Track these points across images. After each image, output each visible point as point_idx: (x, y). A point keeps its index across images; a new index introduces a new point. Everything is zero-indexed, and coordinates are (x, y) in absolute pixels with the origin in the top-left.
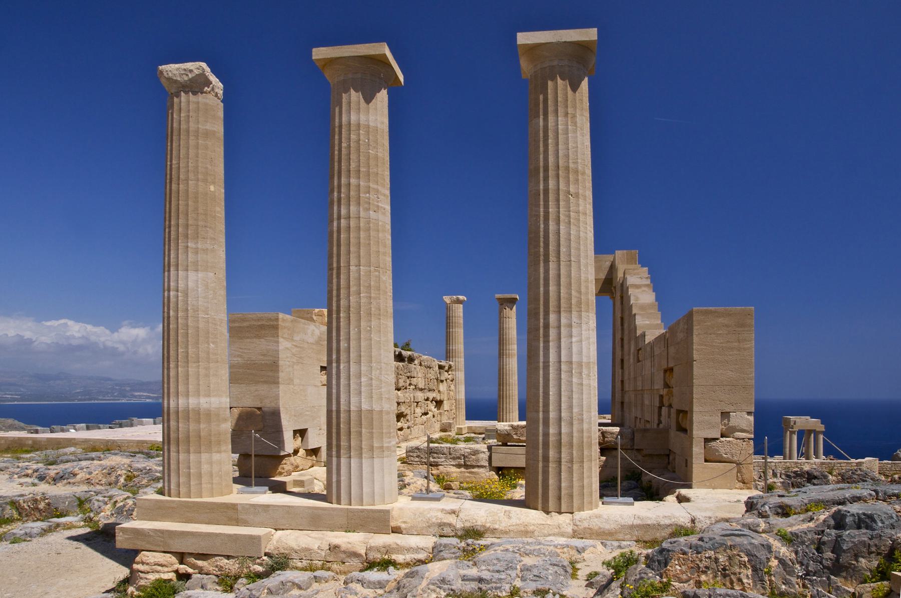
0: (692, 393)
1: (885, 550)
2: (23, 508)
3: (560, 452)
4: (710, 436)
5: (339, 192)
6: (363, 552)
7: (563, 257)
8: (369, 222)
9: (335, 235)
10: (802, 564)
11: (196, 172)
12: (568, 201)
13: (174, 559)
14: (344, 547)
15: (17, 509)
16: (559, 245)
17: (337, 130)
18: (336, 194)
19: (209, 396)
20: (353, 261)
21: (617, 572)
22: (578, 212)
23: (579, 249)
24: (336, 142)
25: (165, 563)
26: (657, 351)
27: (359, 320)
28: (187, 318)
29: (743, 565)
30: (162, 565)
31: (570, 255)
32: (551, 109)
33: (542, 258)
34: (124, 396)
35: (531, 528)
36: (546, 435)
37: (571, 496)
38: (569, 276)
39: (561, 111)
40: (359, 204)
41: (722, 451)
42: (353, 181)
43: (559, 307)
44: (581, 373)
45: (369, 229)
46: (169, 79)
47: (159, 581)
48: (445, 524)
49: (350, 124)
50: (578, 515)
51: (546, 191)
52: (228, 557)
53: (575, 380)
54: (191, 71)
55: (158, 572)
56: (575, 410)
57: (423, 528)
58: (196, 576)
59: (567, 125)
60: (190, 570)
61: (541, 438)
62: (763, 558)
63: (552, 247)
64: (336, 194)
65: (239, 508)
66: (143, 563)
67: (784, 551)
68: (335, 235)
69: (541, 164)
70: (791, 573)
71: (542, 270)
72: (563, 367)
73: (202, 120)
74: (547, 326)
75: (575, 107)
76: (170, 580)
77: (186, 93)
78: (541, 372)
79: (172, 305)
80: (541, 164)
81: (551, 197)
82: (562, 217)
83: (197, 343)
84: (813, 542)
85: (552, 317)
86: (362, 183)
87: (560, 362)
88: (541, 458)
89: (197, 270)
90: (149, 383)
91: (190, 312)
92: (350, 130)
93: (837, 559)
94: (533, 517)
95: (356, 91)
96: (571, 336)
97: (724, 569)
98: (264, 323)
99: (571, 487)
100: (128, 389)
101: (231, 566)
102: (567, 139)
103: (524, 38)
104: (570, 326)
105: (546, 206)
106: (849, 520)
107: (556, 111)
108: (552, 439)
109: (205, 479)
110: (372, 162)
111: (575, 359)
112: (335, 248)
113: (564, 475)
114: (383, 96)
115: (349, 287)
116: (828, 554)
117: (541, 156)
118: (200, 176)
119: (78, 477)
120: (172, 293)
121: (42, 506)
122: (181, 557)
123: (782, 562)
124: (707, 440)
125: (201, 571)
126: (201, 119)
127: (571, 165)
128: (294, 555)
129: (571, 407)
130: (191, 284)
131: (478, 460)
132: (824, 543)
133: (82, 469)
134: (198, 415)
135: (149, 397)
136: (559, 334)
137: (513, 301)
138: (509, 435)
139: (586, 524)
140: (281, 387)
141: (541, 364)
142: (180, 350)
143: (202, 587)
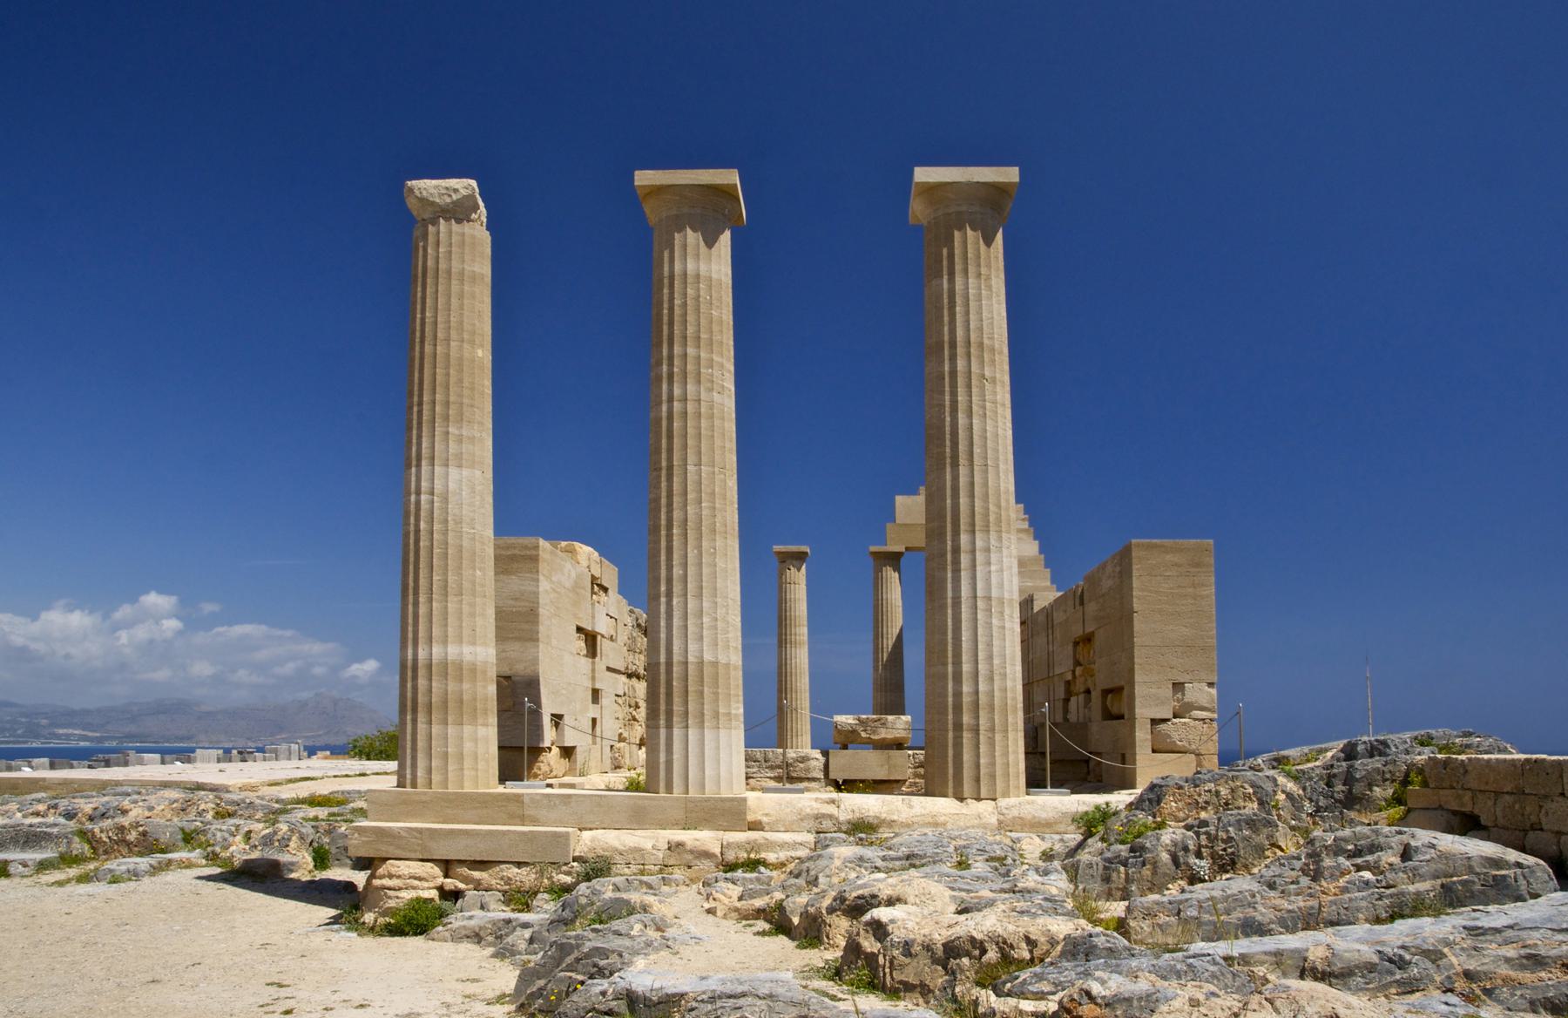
0: (1132, 658)
1: (1399, 776)
2: (99, 841)
3: (977, 717)
4: (1158, 716)
5: (671, 365)
6: (717, 851)
7: (977, 461)
8: (712, 408)
9: (664, 423)
10: (1311, 800)
11: (461, 329)
12: (982, 388)
13: (436, 871)
14: (690, 844)
15: (89, 842)
16: (971, 444)
17: (666, 281)
18: (665, 368)
19: (474, 644)
20: (691, 459)
21: (1089, 834)
22: (995, 402)
23: (997, 451)
24: (666, 298)
25: (424, 875)
26: (1059, 617)
27: (700, 538)
28: (445, 532)
29: (1247, 797)
30: (420, 879)
31: (986, 458)
32: (958, 267)
33: (948, 461)
34: (37, 736)
35: (942, 819)
36: (958, 694)
37: (993, 777)
38: (986, 484)
39: (971, 269)
40: (699, 382)
41: (1175, 736)
42: (691, 351)
43: (973, 525)
44: (1002, 613)
45: (712, 417)
46: (422, 200)
47: (418, 899)
48: (824, 816)
49: (685, 274)
50: (1002, 802)
51: (953, 373)
52: (519, 864)
53: (995, 621)
54: (456, 191)
55: (414, 888)
56: (996, 661)
57: (792, 823)
58: (471, 894)
59: (980, 288)
60: (462, 886)
61: (950, 699)
62: (1270, 789)
63: (962, 447)
64: (665, 368)
65: (526, 800)
66: (391, 876)
67: (1291, 786)
68: (664, 423)
69: (946, 338)
70: (1300, 809)
71: (948, 477)
72: (980, 604)
73: (463, 264)
74: (956, 550)
75: (989, 266)
76: (432, 900)
77: (447, 220)
78: (950, 611)
79: (423, 514)
80: (946, 338)
81: (961, 381)
82: (975, 408)
83: (460, 568)
84: (1321, 778)
85: (964, 538)
86: (702, 355)
87: (975, 597)
88: (950, 726)
89: (460, 466)
90: (86, 712)
91: (451, 525)
92: (685, 283)
93: (1350, 791)
94: (943, 806)
95: (694, 230)
96: (989, 564)
97: (1227, 804)
98: (516, 552)
99: (993, 764)
100: (44, 722)
101: (526, 877)
102: (980, 307)
103: (924, 175)
104: (988, 550)
105: (954, 394)
106: (1360, 748)
107: (966, 271)
108: (966, 700)
109: (467, 763)
110: (715, 328)
111: (994, 594)
112: (664, 441)
113: (983, 748)
114: (726, 238)
115: (685, 493)
116: (1339, 787)
117: (946, 328)
118: (466, 336)
119: (132, 814)
120: (423, 497)
121: (132, 836)
122: (447, 866)
123: (1289, 796)
124: (1154, 722)
125: (478, 886)
126: (467, 258)
127: (986, 341)
128: (618, 859)
129: (990, 657)
130: (452, 486)
131: (808, 770)
132: (1335, 776)
133: (135, 802)
134: (461, 670)
135: (85, 738)
136: (974, 560)
137: (800, 557)
138: (854, 732)
139: (1015, 812)
140: (541, 646)
141: (949, 601)
142: (435, 578)
143: (482, 908)
